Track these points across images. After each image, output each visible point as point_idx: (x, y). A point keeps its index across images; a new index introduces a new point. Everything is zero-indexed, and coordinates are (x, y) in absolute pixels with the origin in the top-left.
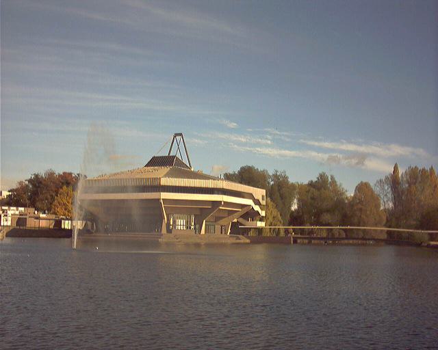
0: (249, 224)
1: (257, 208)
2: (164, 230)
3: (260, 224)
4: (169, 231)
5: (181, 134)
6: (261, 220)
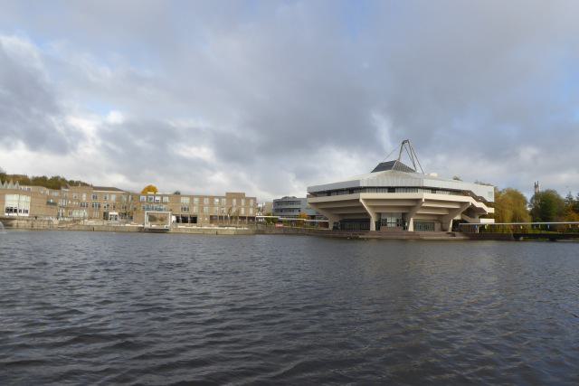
0: (472, 221)
1: (479, 205)
2: (373, 227)
3: (484, 221)
4: (378, 227)
5: (407, 141)
6: (490, 216)
